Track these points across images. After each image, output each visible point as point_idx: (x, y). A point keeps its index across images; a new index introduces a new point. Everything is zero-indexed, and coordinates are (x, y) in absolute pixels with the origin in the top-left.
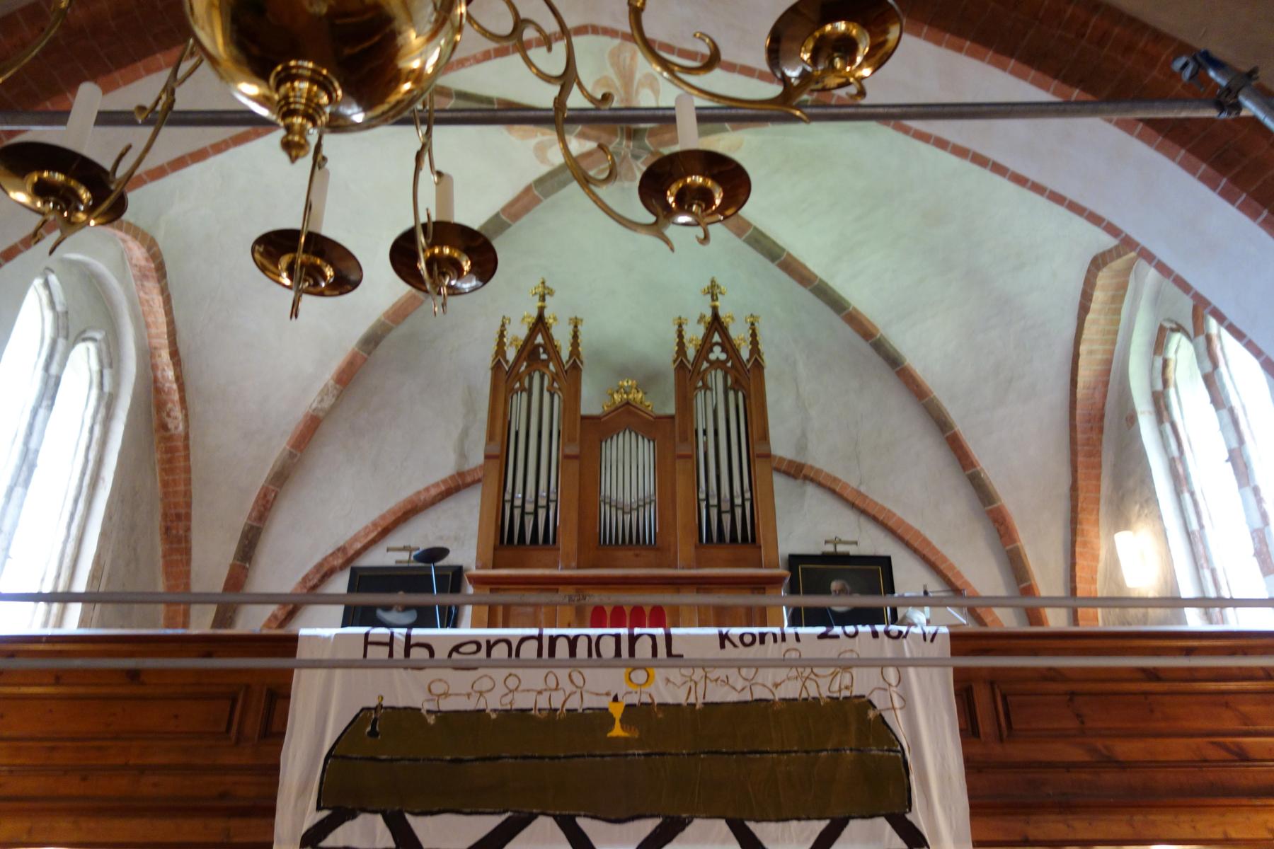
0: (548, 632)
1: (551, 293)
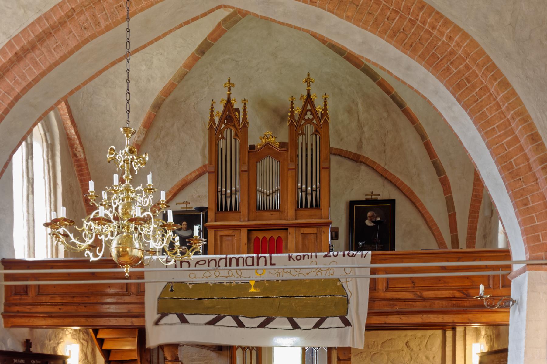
0: (230, 256)
1: (233, 85)
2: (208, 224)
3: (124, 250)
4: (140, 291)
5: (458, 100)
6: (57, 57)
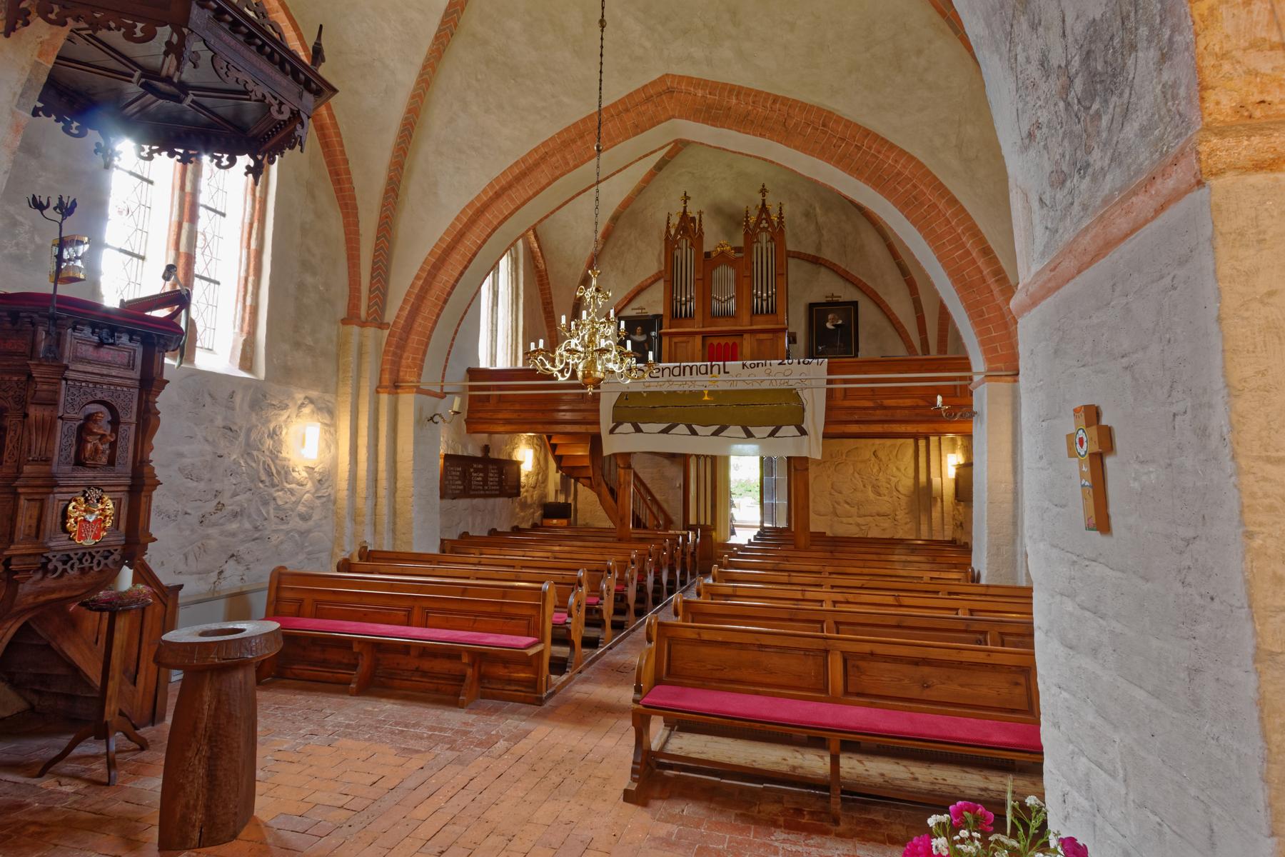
0: (683, 364)
1: (689, 198)
2: (662, 331)
3: (589, 373)
4: (596, 398)
5: (906, 216)
6: (531, 193)
